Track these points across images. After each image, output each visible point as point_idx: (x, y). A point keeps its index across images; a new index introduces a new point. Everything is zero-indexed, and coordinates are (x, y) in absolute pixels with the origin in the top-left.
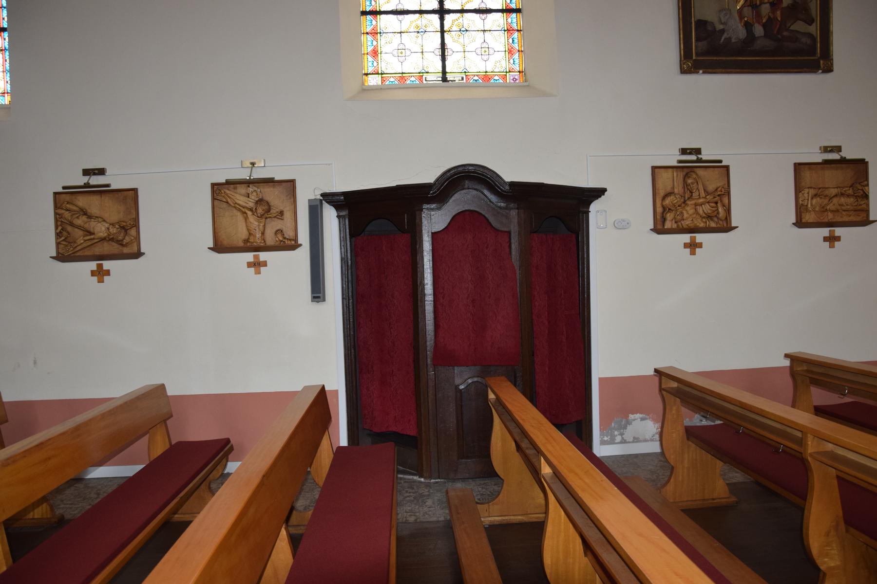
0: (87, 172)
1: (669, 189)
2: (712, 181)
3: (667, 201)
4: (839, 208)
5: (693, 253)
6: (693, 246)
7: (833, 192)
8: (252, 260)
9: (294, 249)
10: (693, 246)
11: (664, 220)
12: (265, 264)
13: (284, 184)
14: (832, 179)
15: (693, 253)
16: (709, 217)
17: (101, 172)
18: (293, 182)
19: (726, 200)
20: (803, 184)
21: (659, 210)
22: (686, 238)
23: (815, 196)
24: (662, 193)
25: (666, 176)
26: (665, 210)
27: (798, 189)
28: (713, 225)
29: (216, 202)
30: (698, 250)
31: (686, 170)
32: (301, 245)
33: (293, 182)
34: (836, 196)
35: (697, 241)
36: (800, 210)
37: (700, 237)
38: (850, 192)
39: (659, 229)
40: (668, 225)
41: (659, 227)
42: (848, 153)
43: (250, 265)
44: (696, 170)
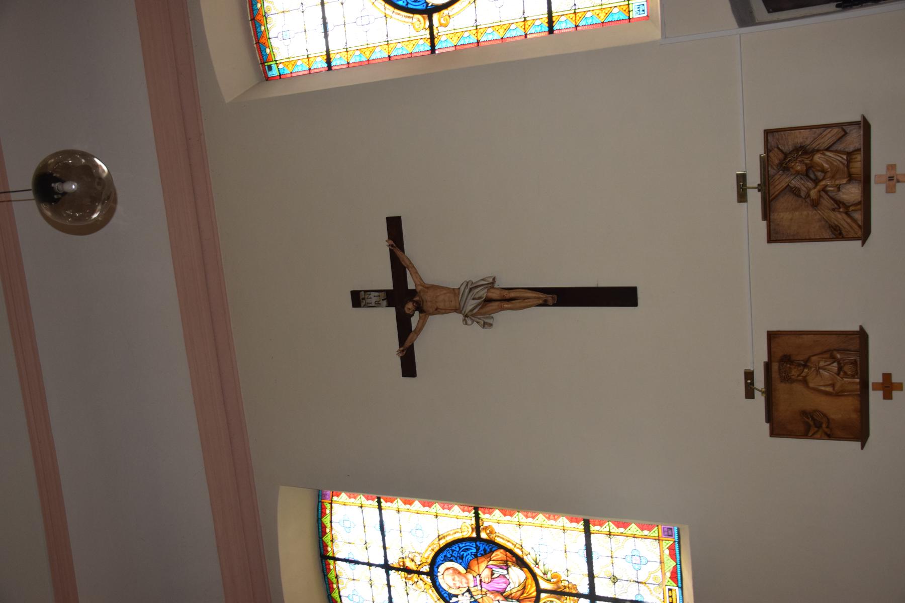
5: (899, 387)
8: (880, 393)
10: (888, 387)
12: (887, 377)
15: (899, 387)
17: (749, 375)
22: (875, 397)
32: (861, 327)
33: (770, 240)
35: (881, 380)
37: (875, 376)
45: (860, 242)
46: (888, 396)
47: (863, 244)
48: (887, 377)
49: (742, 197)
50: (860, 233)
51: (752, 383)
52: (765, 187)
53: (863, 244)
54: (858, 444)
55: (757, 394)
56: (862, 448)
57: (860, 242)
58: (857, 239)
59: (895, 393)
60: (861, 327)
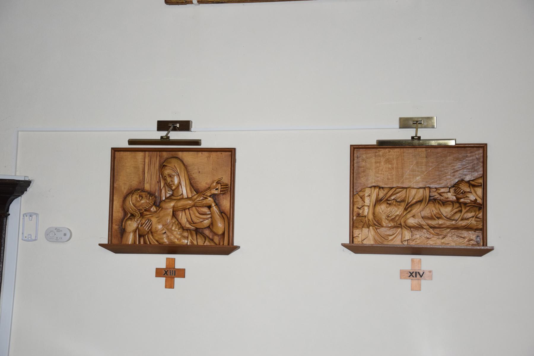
0: (162, 125)
1: (134, 183)
2: (206, 174)
3: (131, 202)
4: (423, 222)
5: (170, 285)
6: (170, 274)
7: (415, 195)
8: (163, 265)
9: (481, 255)
10: (170, 274)
11: (123, 232)
12: (181, 273)
13: (214, 154)
14: (415, 178)
15: (170, 285)
16: (198, 231)
17: (185, 126)
18: (232, 151)
19: (225, 203)
20: (363, 180)
21: (118, 214)
22: (160, 260)
23: (379, 201)
24: (125, 189)
25: (132, 163)
26: (127, 215)
27: (355, 192)
28: (200, 242)
29: (226, 180)
30: (177, 280)
31: (165, 154)
32: (237, 248)
33: (232, 151)
34: (420, 202)
35: (177, 266)
36: (357, 221)
37: (181, 261)
38: (451, 196)
39: (117, 244)
40: (130, 239)
41: (115, 241)
42: (446, 132)
43: (159, 273)
44: (180, 154)
45: (347, 241)
46: (159, 273)
47: (344, 245)
48: (181, 273)
49: (405, 123)
50: (357, 241)
51: (175, 129)
52: (415, 143)
53: (344, 245)
54: (106, 242)
55: (164, 133)
56: (100, 245)
57: (347, 241)
58: (352, 237)
59: (163, 280)
60: (237, 248)
